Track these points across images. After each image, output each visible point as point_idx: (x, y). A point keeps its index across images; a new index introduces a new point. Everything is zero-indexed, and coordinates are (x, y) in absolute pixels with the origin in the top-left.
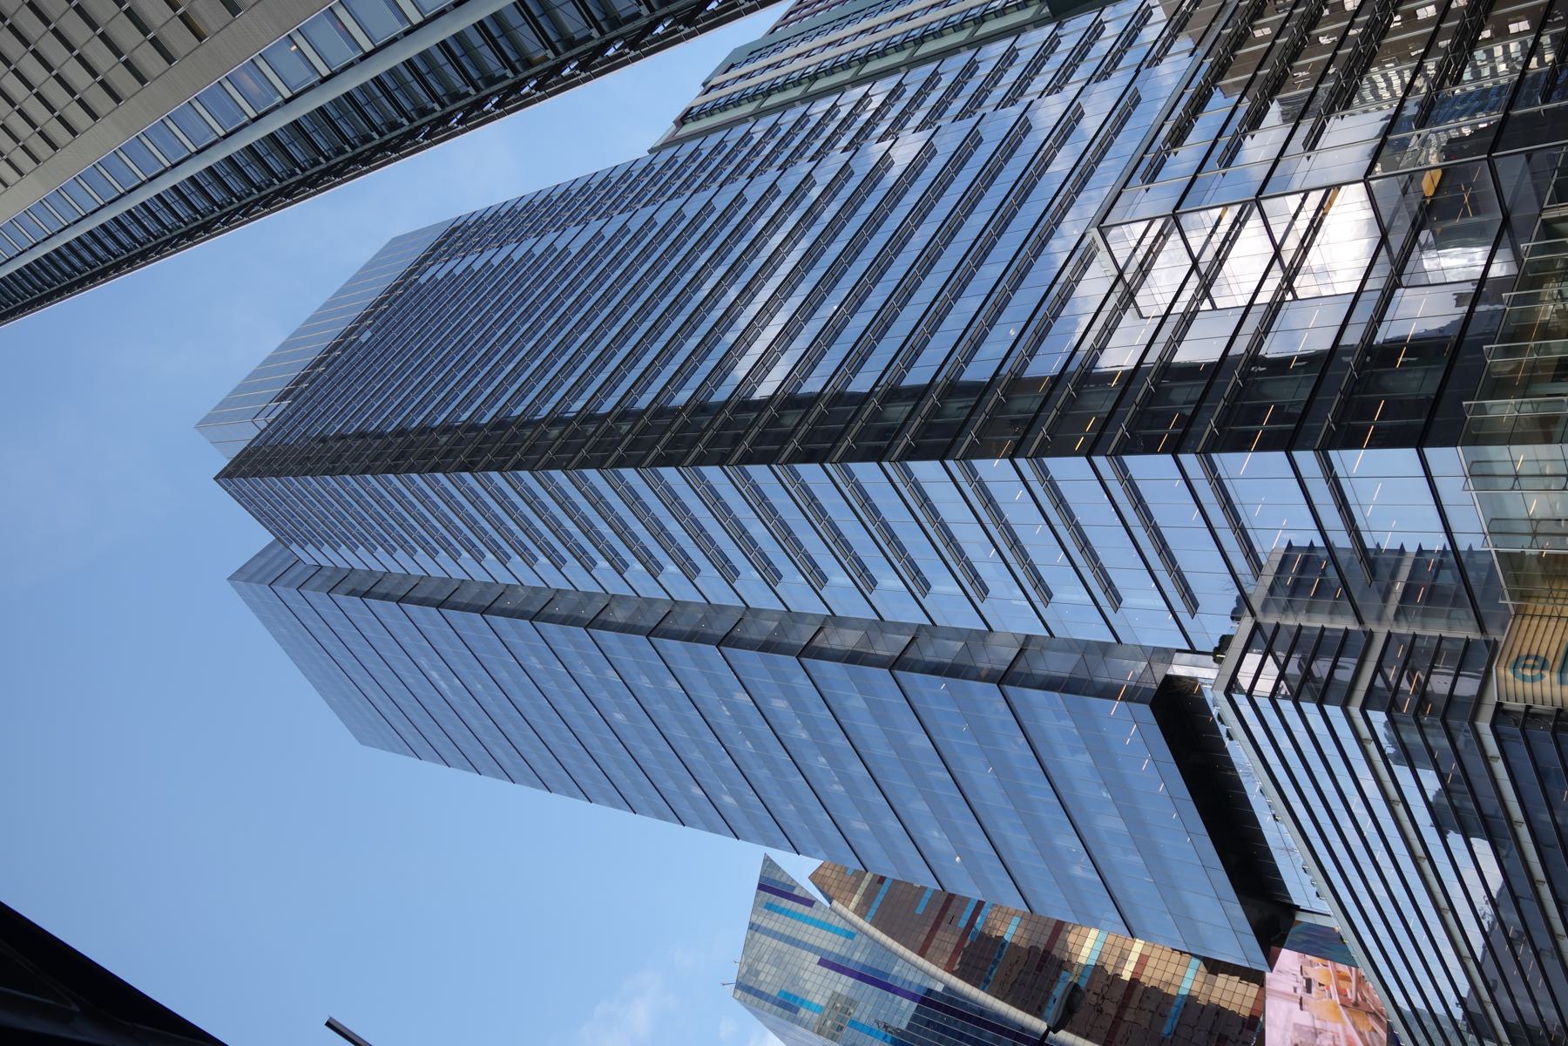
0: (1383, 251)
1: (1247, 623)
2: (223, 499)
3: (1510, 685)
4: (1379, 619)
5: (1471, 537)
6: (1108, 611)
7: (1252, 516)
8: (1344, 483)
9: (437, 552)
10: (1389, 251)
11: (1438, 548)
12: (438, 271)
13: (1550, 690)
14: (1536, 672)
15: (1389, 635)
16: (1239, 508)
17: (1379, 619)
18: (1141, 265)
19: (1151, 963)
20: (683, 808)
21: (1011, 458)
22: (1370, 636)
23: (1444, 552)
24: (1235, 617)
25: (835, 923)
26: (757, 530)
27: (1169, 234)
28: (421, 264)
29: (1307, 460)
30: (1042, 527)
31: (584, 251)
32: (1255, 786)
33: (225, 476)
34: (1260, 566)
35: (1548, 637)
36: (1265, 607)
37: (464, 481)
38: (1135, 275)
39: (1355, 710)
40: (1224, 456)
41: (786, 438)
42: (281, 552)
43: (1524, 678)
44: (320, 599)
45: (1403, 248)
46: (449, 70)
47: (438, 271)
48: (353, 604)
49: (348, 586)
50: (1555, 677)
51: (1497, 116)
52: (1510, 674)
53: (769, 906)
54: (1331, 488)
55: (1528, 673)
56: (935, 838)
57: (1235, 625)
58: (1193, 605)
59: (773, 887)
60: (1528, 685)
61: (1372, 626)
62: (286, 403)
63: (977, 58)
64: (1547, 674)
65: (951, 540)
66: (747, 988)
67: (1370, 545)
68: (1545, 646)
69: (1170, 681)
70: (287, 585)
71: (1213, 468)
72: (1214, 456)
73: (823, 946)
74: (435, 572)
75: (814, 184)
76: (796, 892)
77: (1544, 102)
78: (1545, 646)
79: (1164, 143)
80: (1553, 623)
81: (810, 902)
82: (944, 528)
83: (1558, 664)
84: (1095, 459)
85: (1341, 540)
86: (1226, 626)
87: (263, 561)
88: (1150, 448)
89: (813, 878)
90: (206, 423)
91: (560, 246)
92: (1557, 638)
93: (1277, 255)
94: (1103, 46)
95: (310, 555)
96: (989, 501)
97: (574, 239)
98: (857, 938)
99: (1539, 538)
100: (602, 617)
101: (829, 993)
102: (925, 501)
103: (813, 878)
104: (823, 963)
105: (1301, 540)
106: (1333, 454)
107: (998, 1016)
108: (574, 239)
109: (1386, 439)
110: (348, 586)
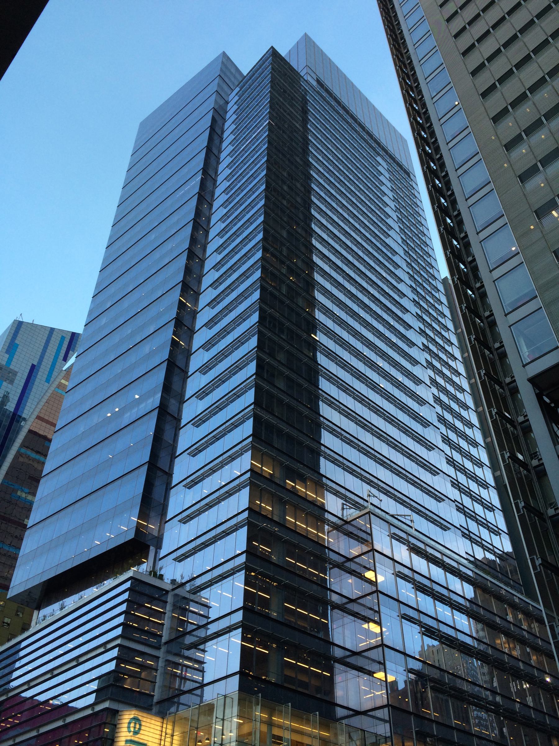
0: (348, 653)
1: (169, 587)
2: (263, 50)
4: (168, 652)
6: (179, 517)
7: (216, 589)
8: (227, 636)
9: (230, 169)
10: (348, 656)
13: (124, 734)
15: (158, 658)
17: (168, 652)
20: (101, 297)
21: (251, 470)
22: (158, 648)
24: (173, 581)
26: (229, 339)
31: (387, 246)
33: (274, 53)
34: (195, 593)
35: (151, 734)
36: (176, 595)
37: (262, 185)
38: (347, 530)
39: (118, 642)
40: (244, 575)
41: (271, 355)
42: (233, 83)
44: (211, 103)
45: (349, 663)
49: (217, 118)
50: (129, 738)
51: (531, 704)
52: (132, 716)
53: (63, 338)
55: (132, 725)
56: (81, 427)
57: (169, 582)
58: (179, 559)
61: (163, 649)
62: (314, 83)
64: (131, 734)
66: (18, 325)
69: (148, 547)
70: (219, 85)
71: (239, 571)
73: (42, 366)
76: (71, 352)
77: (416, 732)
83: (136, 739)
84: (247, 512)
86: (168, 578)
87: (233, 71)
90: (307, 40)
91: (391, 233)
92: (150, 739)
93: (351, 601)
95: (233, 98)
97: (395, 240)
98: (47, 384)
104: (33, 367)
108: (395, 240)
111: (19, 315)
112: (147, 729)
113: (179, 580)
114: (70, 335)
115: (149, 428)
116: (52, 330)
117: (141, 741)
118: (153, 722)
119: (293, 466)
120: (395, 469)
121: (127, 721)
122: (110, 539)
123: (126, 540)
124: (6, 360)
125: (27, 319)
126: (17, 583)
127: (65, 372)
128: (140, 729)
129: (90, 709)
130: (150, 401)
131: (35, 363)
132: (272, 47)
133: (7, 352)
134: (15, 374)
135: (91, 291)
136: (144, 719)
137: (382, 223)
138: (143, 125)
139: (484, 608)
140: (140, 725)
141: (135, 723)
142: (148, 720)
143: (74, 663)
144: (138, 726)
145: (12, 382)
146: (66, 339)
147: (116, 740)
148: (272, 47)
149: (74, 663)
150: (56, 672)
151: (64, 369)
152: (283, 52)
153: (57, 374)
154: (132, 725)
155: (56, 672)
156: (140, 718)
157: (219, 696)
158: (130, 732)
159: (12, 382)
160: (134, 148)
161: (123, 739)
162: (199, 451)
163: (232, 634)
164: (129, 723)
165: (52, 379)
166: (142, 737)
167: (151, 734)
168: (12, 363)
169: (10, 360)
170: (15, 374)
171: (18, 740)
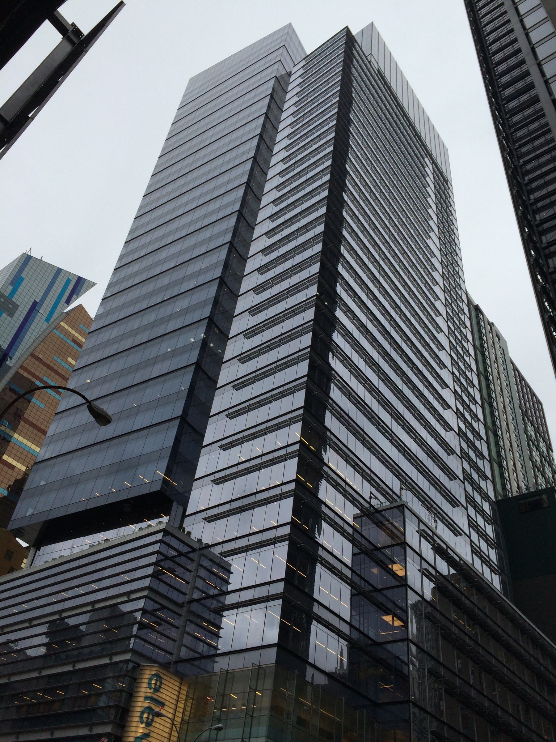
3: (148, 672)
5: (221, 664)
7: (253, 557)
11: (220, 647)
12: (429, 169)
14: (153, 686)
16: (258, 550)
18: (381, 522)
19: (10, 471)
21: (300, 442)
23: (216, 648)
25: (55, 314)
27: (392, 538)
28: (434, 163)
29: (279, 588)
30: (260, 452)
32: (114, 535)
35: (169, 694)
43: (151, 679)
46: (544, 192)
47: (429, 169)
48: (267, 89)
50: (149, 695)
52: (154, 672)
53: (69, 281)
54: (262, 598)
58: (209, 520)
59: (79, 285)
60: (146, 681)
63: (485, 460)
64: (152, 691)
65: (260, 405)
67: (225, 613)
68: (165, 692)
69: (172, 502)
72: (287, 542)
74: (279, 137)
75: (441, 369)
76: (74, 296)
78: (165, 692)
79: (438, 544)
80: (175, 697)
81: (68, 302)
82: (269, 401)
83: (155, 697)
84: (294, 483)
85: (230, 599)
88: (296, 511)
89: (80, 307)
91: (432, 234)
92: (168, 698)
94: (442, 531)
96: (278, 427)
98: (46, 323)
99: (221, 697)
100: (242, 219)
101: (18, 303)
102: (283, 395)
103: (80, 307)
104: (35, 304)
105: (232, 578)
106: (280, 601)
107: (529, 155)
109: (283, 629)
110: (279, 89)
111: (28, 250)
112: (166, 688)
113: (205, 541)
114: (76, 279)
115: (183, 382)
116: (59, 270)
117: (160, 699)
118: (172, 681)
119: (306, 455)
120: (382, 488)
121: (148, 676)
122: (111, 493)
123: (88, 508)
124: (9, 291)
125: (35, 254)
126: (18, 517)
127: (65, 315)
128: (160, 687)
129: (71, 666)
130: (186, 356)
131: (38, 301)
132: (347, 27)
133: (12, 283)
134: (16, 307)
135: (124, 236)
136: (165, 677)
137: (375, 232)
138: (193, 81)
139: (445, 667)
140: (161, 683)
141: (157, 680)
142: (168, 679)
143: (27, 625)
144: (158, 684)
145: (11, 314)
146: (72, 282)
147: (135, 694)
148: (347, 27)
149: (27, 625)
150: (35, 623)
151: (65, 311)
152: (354, 32)
153: (55, 318)
154: (153, 682)
155: (35, 623)
156: (162, 675)
157: (254, 665)
158: (150, 688)
159: (11, 314)
160: (181, 103)
161: (142, 694)
162: (238, 414)
163: (271, 603)
164: (151, 679)
165: (52, 320)
166: (161, 695)
167: (169, 694)
168: (15, 296)
169: (13, 292)
170: (16, 307)
171: (13, 679)
